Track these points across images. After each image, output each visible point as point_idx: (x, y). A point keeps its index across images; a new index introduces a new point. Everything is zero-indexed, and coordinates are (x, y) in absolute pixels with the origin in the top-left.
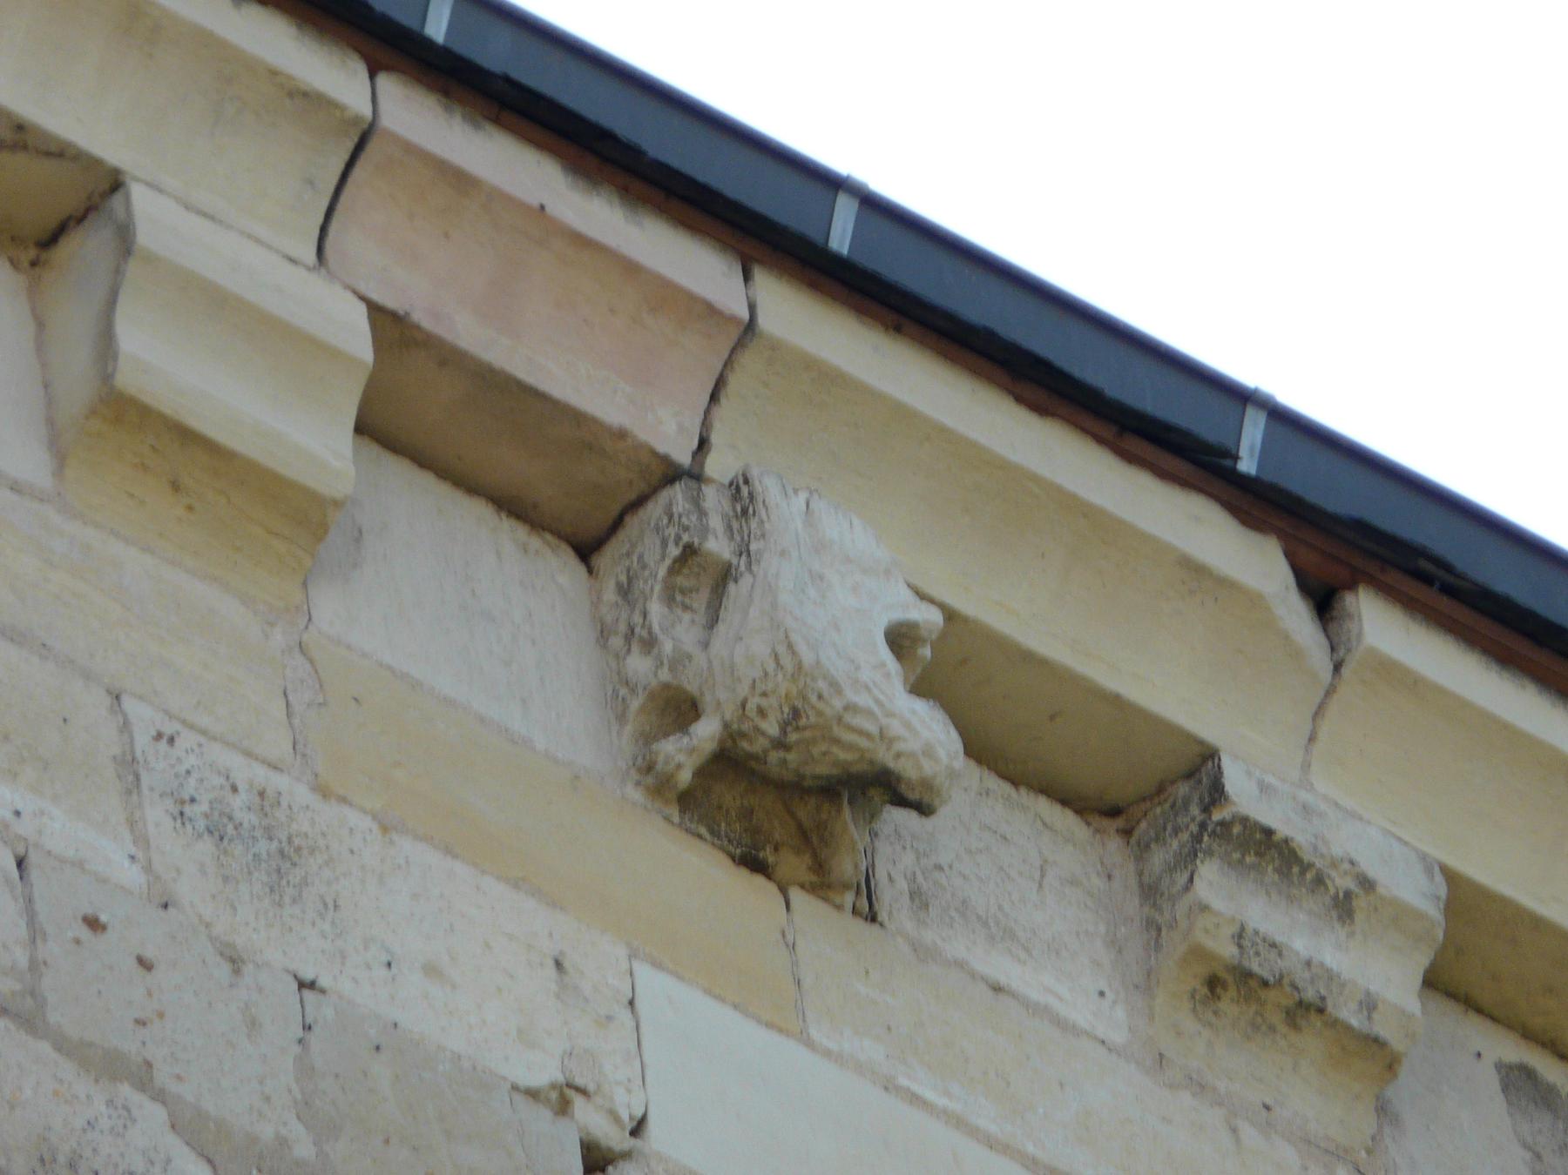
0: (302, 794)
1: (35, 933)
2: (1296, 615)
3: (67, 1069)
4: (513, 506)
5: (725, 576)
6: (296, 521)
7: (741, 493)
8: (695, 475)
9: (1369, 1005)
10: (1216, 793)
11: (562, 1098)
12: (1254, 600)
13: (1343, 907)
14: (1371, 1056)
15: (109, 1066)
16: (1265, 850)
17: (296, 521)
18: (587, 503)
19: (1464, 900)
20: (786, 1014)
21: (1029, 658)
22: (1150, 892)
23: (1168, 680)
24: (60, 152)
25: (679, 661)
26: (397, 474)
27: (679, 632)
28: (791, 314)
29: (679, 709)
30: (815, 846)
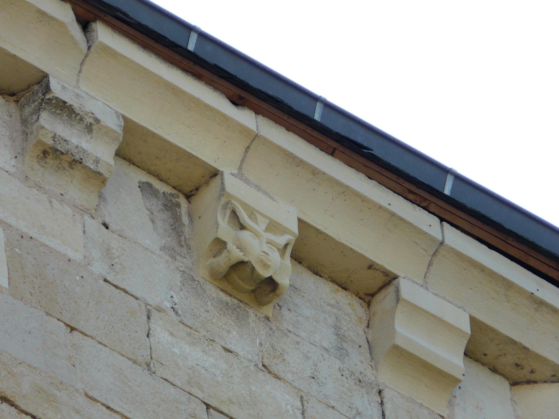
2: (76, 30)
9: (97, 161)
10: (48, 89)
12: (62, 24)
13: (89, 128)
14: (97, 178)
16: (63, 109)
19: (130, 127)
22: (24, 122)
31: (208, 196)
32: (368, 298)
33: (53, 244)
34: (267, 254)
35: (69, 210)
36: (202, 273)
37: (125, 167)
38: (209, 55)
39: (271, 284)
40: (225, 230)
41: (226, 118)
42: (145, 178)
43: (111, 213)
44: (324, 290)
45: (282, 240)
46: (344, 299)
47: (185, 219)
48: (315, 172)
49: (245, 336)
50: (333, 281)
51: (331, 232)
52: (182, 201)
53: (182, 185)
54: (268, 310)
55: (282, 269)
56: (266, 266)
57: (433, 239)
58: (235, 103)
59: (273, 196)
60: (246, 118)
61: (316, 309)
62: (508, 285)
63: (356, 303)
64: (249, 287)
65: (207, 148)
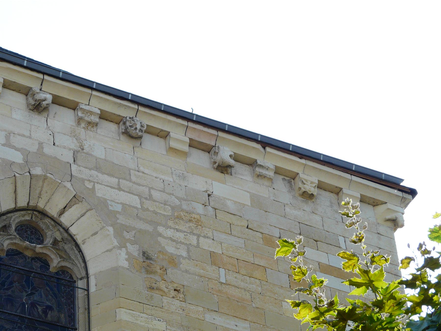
0: (186, 173)
1: (164, 185)
2: (262, 149)
3: (167, 195)
4: (203, 150)
5: (218, 153)
6: (185, 154)
7: (218, 147)
8: (215, 146)
9: (270, 176)
10: (257, 163)
11: (206, 191)
12: (258, 149)
13: (267, 169)
14: (270, 179)
15: (170, 194)
16: (261, 166)
17: (185, 154)
18: (208, 149)
19: (276, 167)
20: (224, 183)
21: (107, 112)
22: (253, 170)
23: (252, 155)
24: (165, 131)
25: (215, 159)
26: (102, 120)
27: (215, 157)
28: (221, 134)
29: (215, 163)
30: (227, 171)
31: (297, 179)
32: (337, 194)
33: (261, 194)
34: (311, 188)
35: (265, 187)
36: (297, 195)
37: (277, 175)
38: (327, 160)
39: (312, 195)
40: (301, 185)
41: (298, 162)
42: (283, 177)
43: (275, 186)
44: (327, 194)
45: (314, 185)
46: (332, 195)
47: (293, 184)
48: (320, 170)
49: (308, 207)
50: (329, 191)
51: (326, 182)
52: (292, 180)
53: (291, 178)
54: (314, 200)
55: (315, 191)
56: (310, 191)
57: (349, 179)
58: (300, 158)
59: (310, 176)
60: (303, 161)
61: (325, 198)
62: (286, 158)
63: (335, 195)
64: (308, 196)
65: (294, 169)
